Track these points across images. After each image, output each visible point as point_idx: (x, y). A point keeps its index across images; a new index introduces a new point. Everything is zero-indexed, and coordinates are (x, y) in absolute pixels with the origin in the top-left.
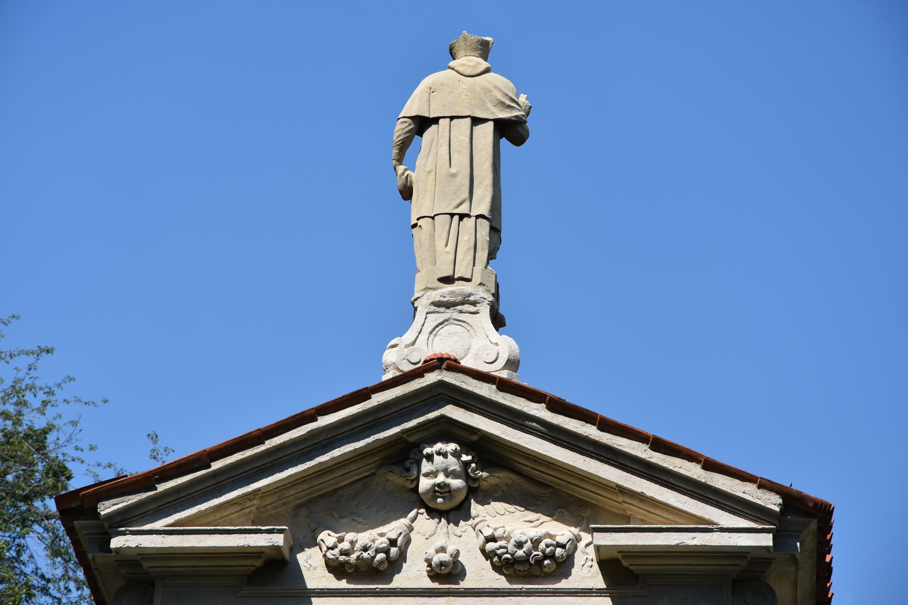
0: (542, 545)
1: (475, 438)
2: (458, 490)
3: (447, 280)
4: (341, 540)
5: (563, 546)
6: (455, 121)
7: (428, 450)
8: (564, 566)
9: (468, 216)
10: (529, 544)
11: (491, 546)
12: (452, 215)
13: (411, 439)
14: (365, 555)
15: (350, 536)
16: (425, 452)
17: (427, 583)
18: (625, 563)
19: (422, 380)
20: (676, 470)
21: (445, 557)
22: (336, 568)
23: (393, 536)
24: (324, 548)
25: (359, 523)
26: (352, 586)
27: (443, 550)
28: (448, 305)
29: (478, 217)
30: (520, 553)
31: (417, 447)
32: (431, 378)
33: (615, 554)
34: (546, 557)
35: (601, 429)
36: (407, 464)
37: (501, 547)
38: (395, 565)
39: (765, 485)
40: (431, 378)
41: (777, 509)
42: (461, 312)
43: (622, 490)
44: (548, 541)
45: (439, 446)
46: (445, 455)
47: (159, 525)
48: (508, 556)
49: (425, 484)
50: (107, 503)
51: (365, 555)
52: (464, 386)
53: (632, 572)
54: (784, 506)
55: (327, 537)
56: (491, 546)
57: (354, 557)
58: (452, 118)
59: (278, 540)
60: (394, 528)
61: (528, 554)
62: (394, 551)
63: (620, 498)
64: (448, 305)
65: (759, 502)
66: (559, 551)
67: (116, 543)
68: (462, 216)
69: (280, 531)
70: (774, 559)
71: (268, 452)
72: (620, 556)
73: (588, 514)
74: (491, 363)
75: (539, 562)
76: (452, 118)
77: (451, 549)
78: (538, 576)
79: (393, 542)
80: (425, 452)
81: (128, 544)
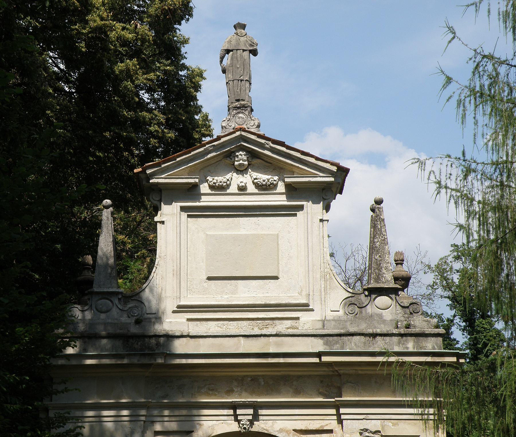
0: (270, 181)
1: (250, 150)
2: (246, 165)
3: (238, 100)
4: (213, 179)
5: (276, 181)
6: (238, 51)
7: (237, 154)
8: (275, 186)
9: (243, 80)
10: (267, 181)
11: (256, 181)
12: (238, 80)
13: (232, 150)
14: (221, 184)
15: (216, 178)
16: (236, 154)
17: (237, 191)
18: (293, 185)
19: (235, 134)
20: (308, 160)
21: (243, 184)
22: (212, 187)
23: (228, 178)
24: (209, 182)
25: (218, 174)
26: (213, 192)
27: (241, 182)
28: (239, 108)
29: (246, 80)
30: (264, 183)
31: (234, 152)
32: (238, 133)
33: (290, 183)
34: (271, 184)
35: (287, 149)
36: (231, 157)
37: (259, 181)
38: (228, 186)
39: (332, 164)
40: (238, 133)
41: (336, 171)
42: (242, 110)
43: (292, 165)
44: (272, 179)
45: (241, 153)
46: (242, 155)
47: (163, 176)
48: (260, 184)
49: (236, 163)
50: (149, 170)
51: (221, 184)
52: (248, 136)
53: (295, 188)
54: (337, 170)
55: (210, 178)
56: (256, 181)
57: (217, 184)
58: (237, 50)
59: (197, 180)
60: (228, 176)
61: (266, 183)
62: (228, 182)
63: (292, 167)
64: (239, 108)
65: (330, 169)
66: (275, 182)
67: (151, 181)
68: (241, 80)
69: (197, 178)
70: (174, 312)
71: (192, 155)
72: (292, 183)
73: (282, 171)
74: (252, 126)
75: (269, 185)
76: (237, 50)
77: (245, 182)
78: (269, 189)
79: (228, 180)
80: (236, 154)
81: (155, 181)
